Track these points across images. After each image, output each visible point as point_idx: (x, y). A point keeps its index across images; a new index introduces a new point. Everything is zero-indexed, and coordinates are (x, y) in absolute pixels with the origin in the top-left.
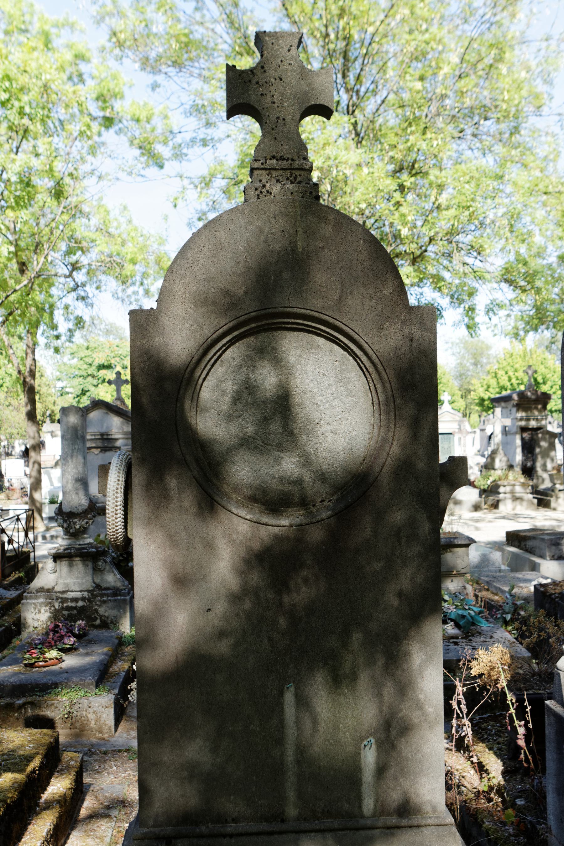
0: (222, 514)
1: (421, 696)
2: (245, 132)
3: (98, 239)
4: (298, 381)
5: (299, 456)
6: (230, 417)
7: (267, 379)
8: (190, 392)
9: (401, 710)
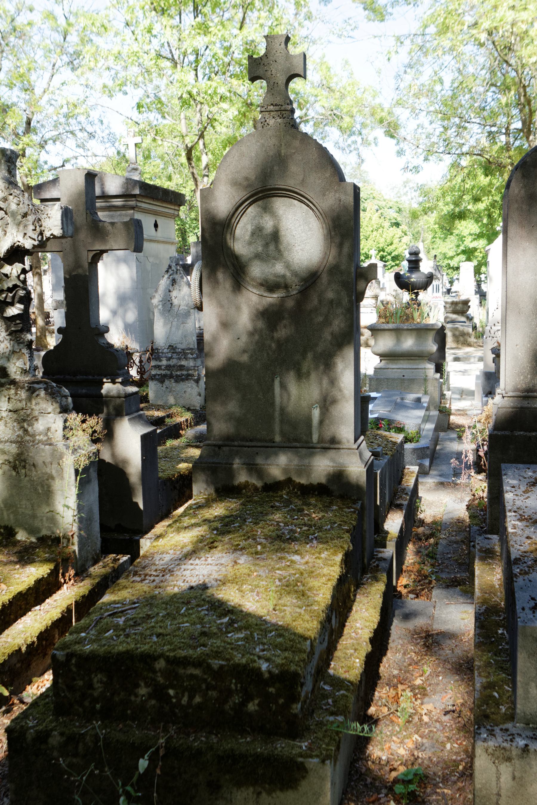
0: (244, 292)
1: (342, 385)
2: (258, 91)
3: (319, 94)
4: (284, 223)
5: (285, 262)
6: (250, 243)
7: (268, 224)
8: (230, 230)
9: (332, 392)
